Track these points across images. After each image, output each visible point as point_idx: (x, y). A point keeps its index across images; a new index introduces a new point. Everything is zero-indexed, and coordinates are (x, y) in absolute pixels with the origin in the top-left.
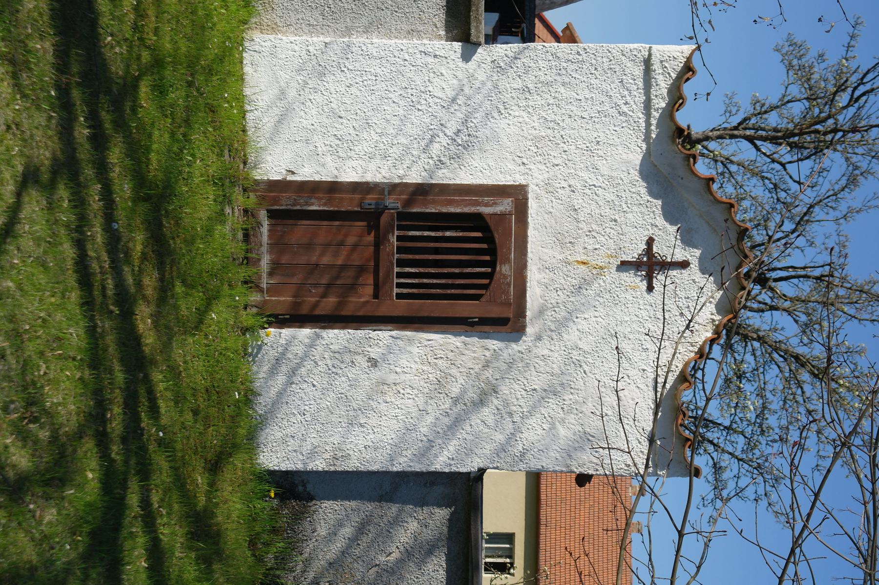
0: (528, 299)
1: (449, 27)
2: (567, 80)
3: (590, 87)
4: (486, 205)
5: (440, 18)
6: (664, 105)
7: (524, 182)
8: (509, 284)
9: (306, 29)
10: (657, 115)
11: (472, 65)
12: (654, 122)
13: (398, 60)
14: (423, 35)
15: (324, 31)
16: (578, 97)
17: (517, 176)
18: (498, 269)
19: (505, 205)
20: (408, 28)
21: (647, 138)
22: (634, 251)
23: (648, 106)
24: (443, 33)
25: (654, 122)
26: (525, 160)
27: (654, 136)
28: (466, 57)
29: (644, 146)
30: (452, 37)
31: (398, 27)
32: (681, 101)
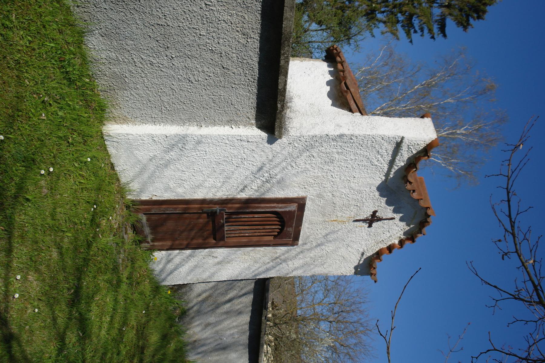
0: (301, 233)
1: (258, 119)
2: (340, 151)
3: (355, 154)
4: (280, 208)
5: (252, 113)
6: (403, 164)
7: (305, 195)
8: (291, 234)
9: (150, 120)
10: (396, 168)
11: (276, 146)
12: (393, 170)
13: (221, 144)
14: (239, 122)
15: (164, 121)
16: (346, 159)
17: (301, 193)
18: (285, 229)
19: (293, 207)
20: (228, 119)
21: (387, 175)
22: (367, 214)
23: (392, 163)
24: (254, 122)
25: (393, 170)
26: (306, 187)
27: (391, 176)
28: (271, 140)
29: (384, 178)
30: (261, 127)
31: (220, 119)
32: (415, 169)
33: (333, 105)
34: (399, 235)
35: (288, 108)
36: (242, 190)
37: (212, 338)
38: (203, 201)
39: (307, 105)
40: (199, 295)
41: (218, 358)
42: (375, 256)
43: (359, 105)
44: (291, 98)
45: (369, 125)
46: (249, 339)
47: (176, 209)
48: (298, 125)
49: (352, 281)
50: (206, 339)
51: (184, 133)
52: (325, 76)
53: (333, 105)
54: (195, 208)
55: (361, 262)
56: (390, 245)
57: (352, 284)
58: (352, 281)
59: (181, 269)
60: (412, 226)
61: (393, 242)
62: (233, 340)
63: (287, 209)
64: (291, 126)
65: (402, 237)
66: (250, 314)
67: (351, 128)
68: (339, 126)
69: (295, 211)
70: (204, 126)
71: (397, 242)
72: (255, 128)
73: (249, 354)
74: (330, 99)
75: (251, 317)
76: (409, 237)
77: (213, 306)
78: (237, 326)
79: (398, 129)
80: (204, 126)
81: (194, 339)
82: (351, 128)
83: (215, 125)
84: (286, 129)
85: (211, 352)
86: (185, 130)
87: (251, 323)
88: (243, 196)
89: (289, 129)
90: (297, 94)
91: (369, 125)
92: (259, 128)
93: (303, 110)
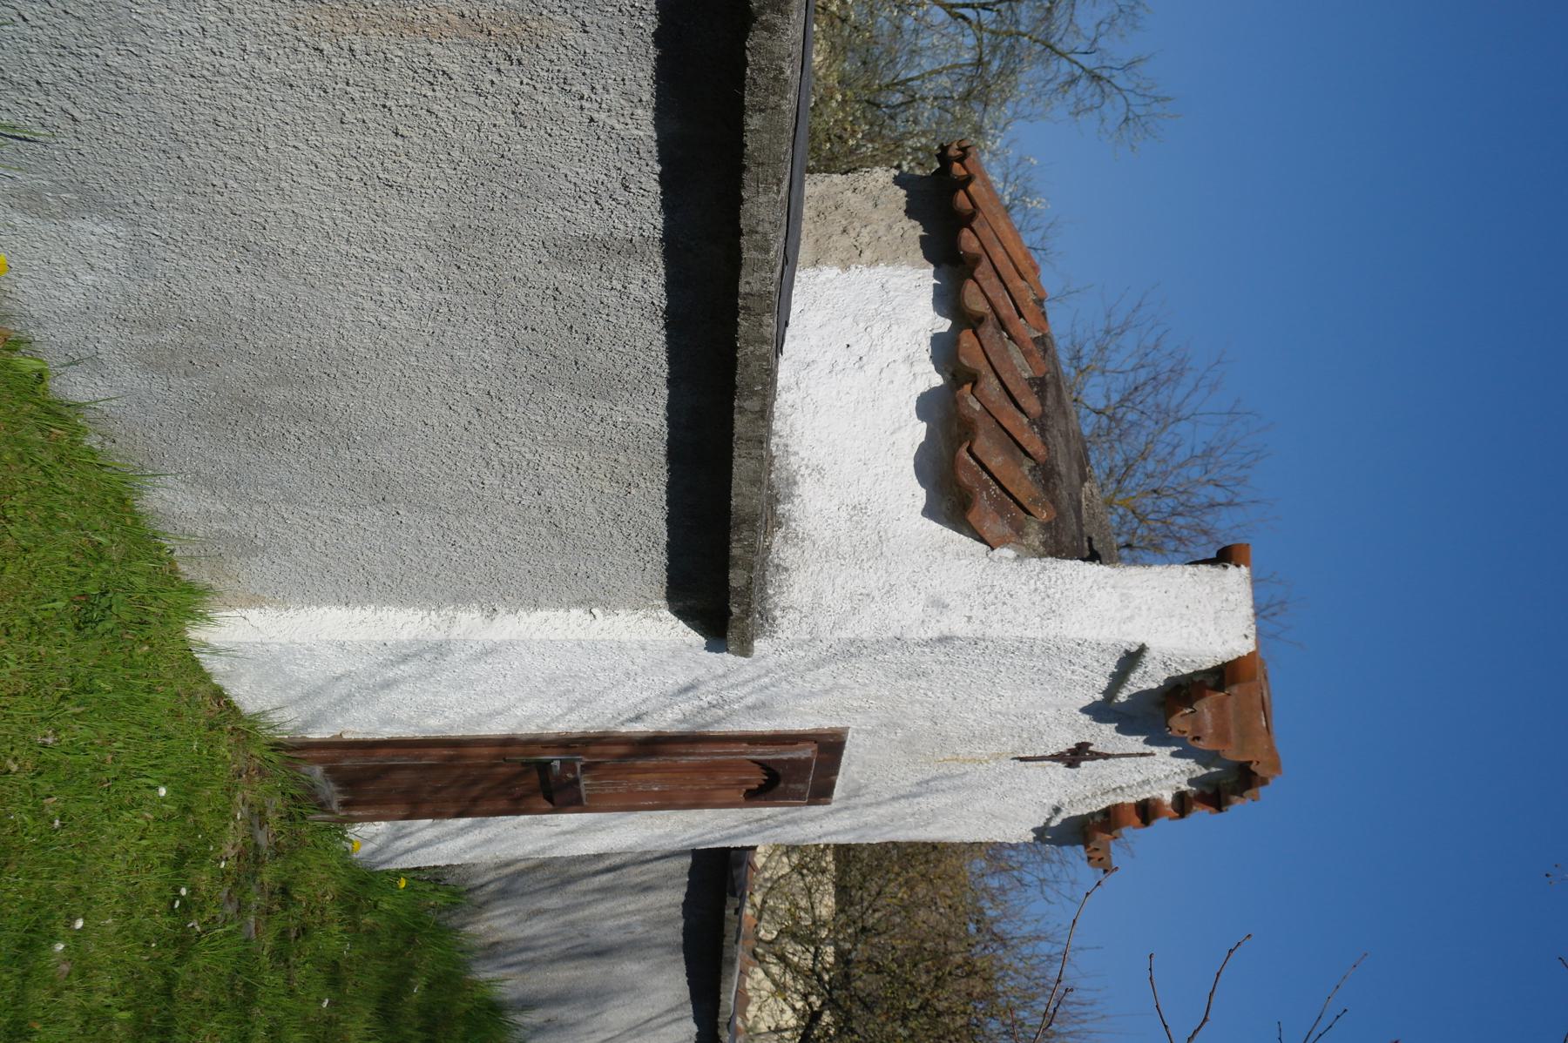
19: (806, 752)
24: (663, 603)
33: (928, 512)
34: (1173, 782)
35: (780, 525)
36: (638, 718)
37: (557, 934)
38: (507, 742)
39: (844, 514)
40: (508, 914)
41: (578, 973)
42: (1098, 819)
43: (1020, 497)
44: (791, 482)
45: (1037, 598)
46: (684, 935)
47: (419, 757)
48: (807, 599)
49: (1185, 412)
50: (534, 938)
51: (438, 636)
52: (918, 368)
53: (928, 512)
54: (479, 756)
55: (1053, 824)
56: (1146, 801)
57: (1183, 428)
58: (1185, 412)
59: (441, 846)
60: (1214, 770)
61: (1155, 794)
62: (629, 937)
63: (785, 757)
64: (783, 601)
65: (1184, 787)
66: (685, 890)
67: (978, 613)
68: (940, 605)
69: (808, 761)
70: (502, 611)
71: (1168, 797)
72: (667, 613)
73: (687, 963)
74: (922, 482)
75: (687, 895)
76: (1208, 791)
77: (557, 880)
78: (639, 911)
79: (1131, 618)
80: (502, 611)
81: (495, 939)
82: (978, 613)
83: (536, 605)
84: (765, 615)
85: (552, 961)
86: (444, 627)
87: (690, 906)
88: (640, 728)
89: (778, 613)
90: (814, 462)
91: (1037, 598)
92: (681, 614)
93: (828, 533)
